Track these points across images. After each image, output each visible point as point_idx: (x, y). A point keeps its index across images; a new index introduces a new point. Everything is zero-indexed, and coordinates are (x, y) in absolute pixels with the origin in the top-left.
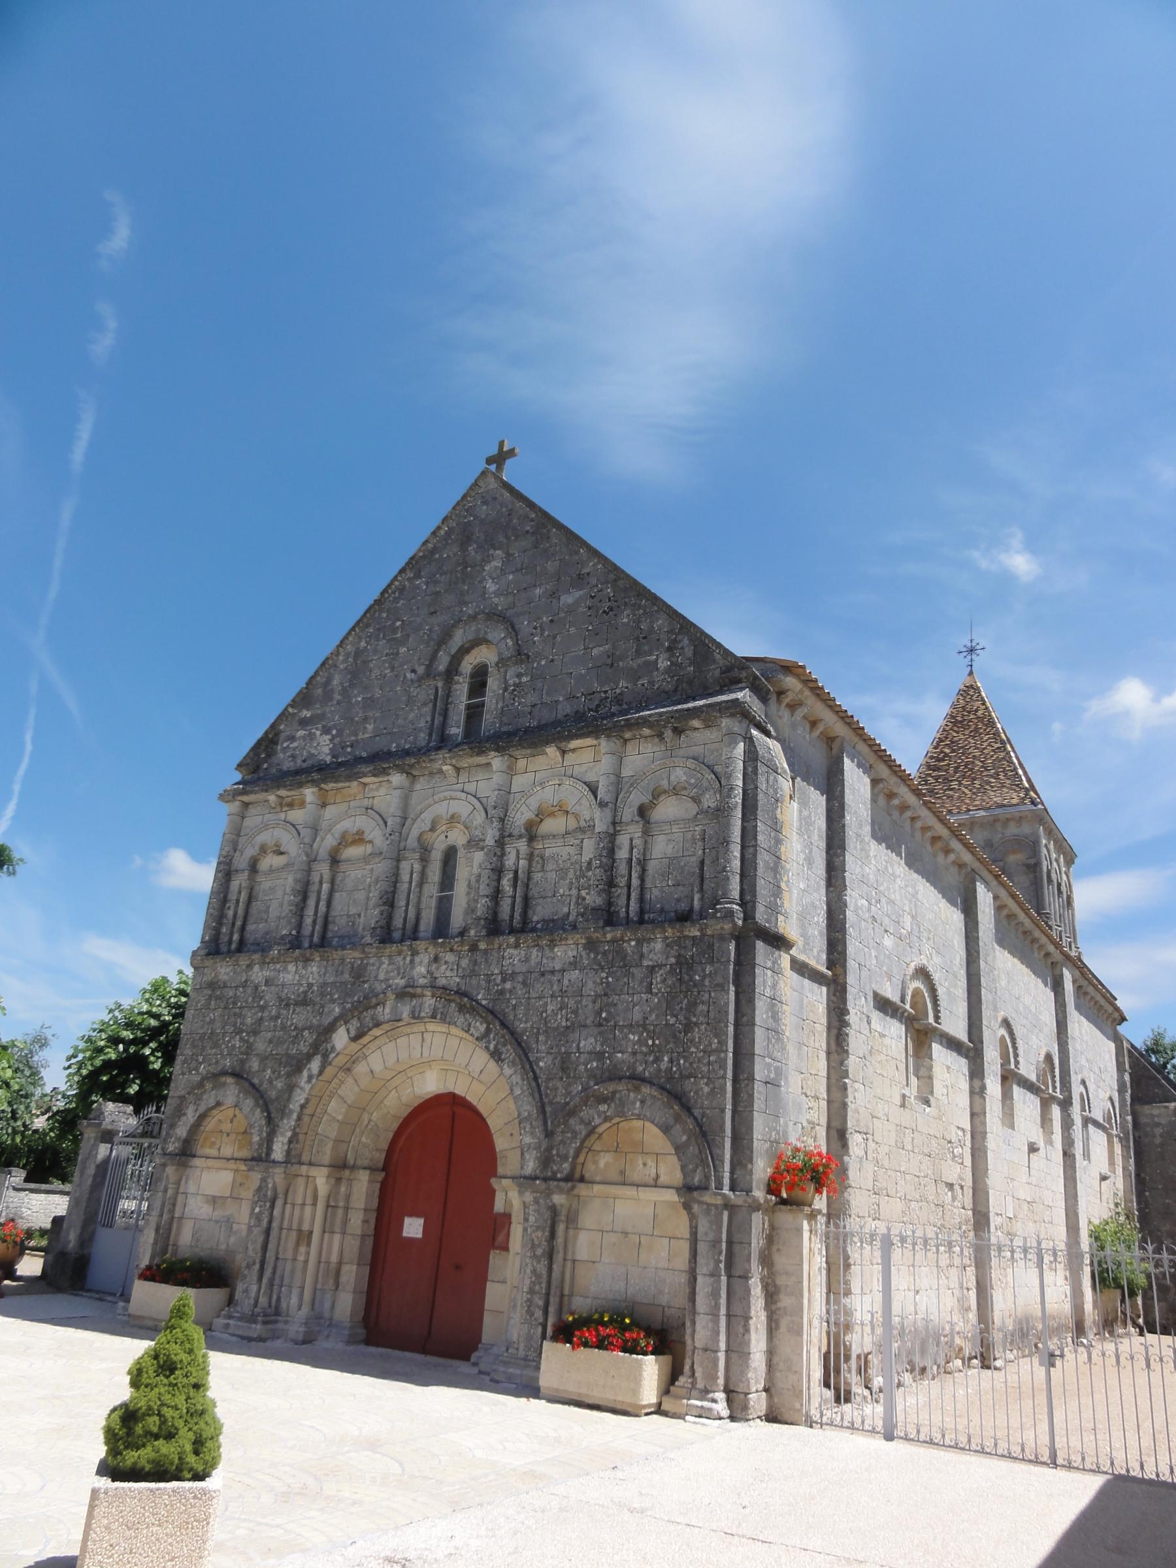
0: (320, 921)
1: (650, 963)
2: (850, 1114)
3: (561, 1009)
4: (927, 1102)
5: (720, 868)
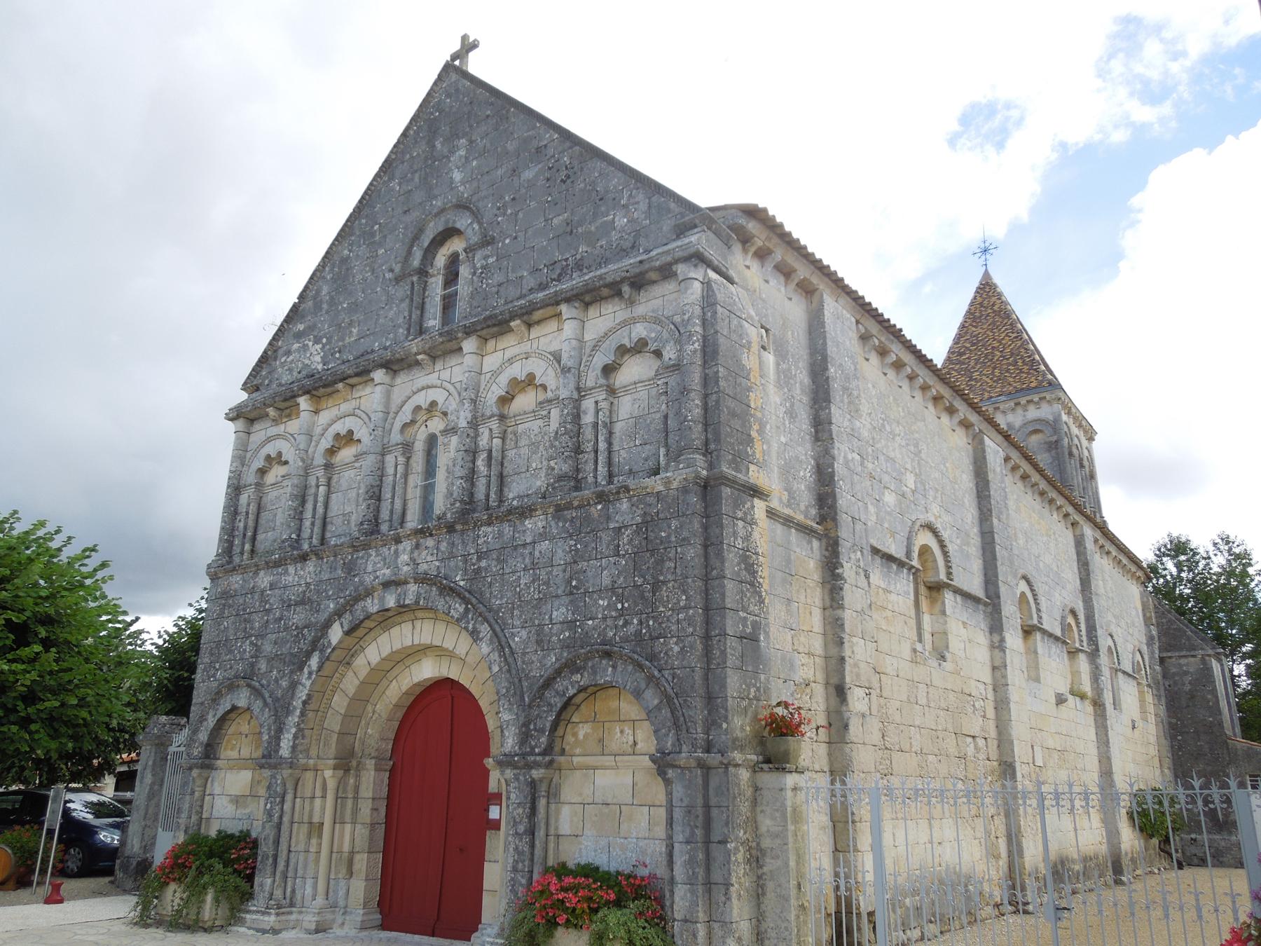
0: (318, 523)
1: (617, 525)
2: (848, 668)
3: (533, 581)
4: (943, 658)
5: (682, 418)
